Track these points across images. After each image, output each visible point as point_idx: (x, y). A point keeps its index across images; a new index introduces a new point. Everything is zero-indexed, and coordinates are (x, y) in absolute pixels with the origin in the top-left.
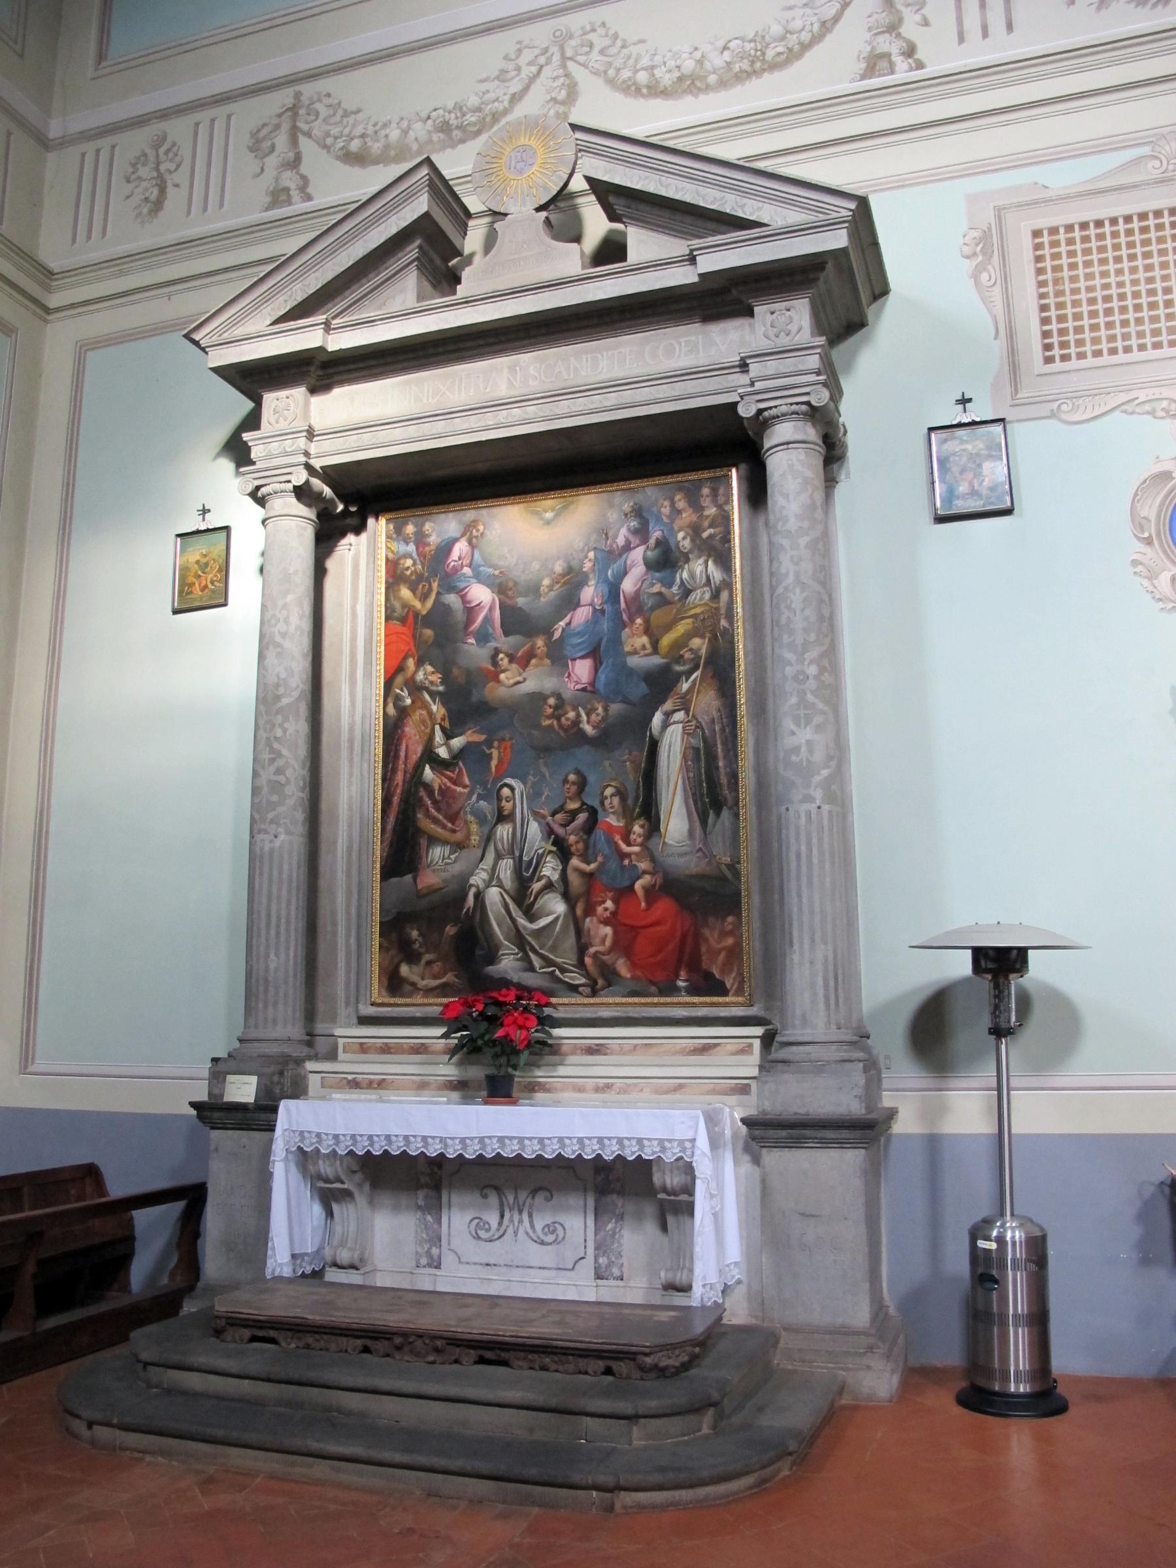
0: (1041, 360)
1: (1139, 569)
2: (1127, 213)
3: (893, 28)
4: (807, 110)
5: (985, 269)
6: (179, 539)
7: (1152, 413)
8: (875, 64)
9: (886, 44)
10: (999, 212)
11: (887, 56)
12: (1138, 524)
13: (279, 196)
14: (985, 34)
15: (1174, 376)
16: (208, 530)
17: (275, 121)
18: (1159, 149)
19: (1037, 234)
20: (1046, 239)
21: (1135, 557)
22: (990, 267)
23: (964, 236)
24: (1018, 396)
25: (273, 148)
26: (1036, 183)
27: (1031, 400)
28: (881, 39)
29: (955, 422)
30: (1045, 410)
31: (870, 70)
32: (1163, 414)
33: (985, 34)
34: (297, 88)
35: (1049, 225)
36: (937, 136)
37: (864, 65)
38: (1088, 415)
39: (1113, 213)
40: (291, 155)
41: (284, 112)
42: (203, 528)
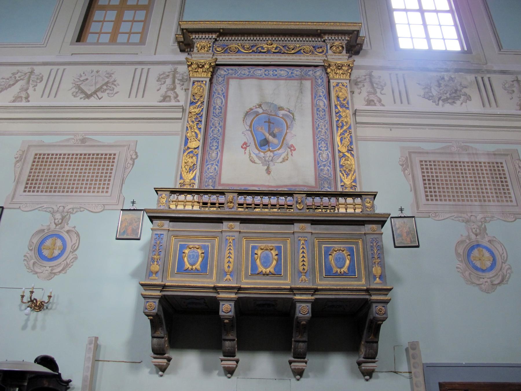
0: (23, 190)
1: (459, 270)
2: (77, 153)
3: (375, 93)
4: (432, 114)
5: (407, 170)
6: (122, 211)
7: (459, 221)
8: (166, 99)
9: (372, 97)
10: (410, 153)
11: (170, 97)
12: (458, 254)
13: (165, 98)
14: (402, 103)
15: (520, 213)
16: (134, 210)
17: (167, 74)
18: (76, 137)
19: (421, 161)
20: (38, 156)
21: (458, 266)
22: (408, 169)
23: (400, 159)
24: (13, 201)
25: (165, 82)
26: (42, 141)
27: (108, 204)
28: (371, 96)
29: (399, 216)
30: (17, 206)
31: (164, 100)
32: (462, 221)
33: (402, 103)
34: (176, 66)
35: (56, 153)
36: (102, 123)
37: (162, 98)
38: (442, 218)
39: (102, 152)
40: (172, 87)
41: (171, 72)
42: (132, 208)
